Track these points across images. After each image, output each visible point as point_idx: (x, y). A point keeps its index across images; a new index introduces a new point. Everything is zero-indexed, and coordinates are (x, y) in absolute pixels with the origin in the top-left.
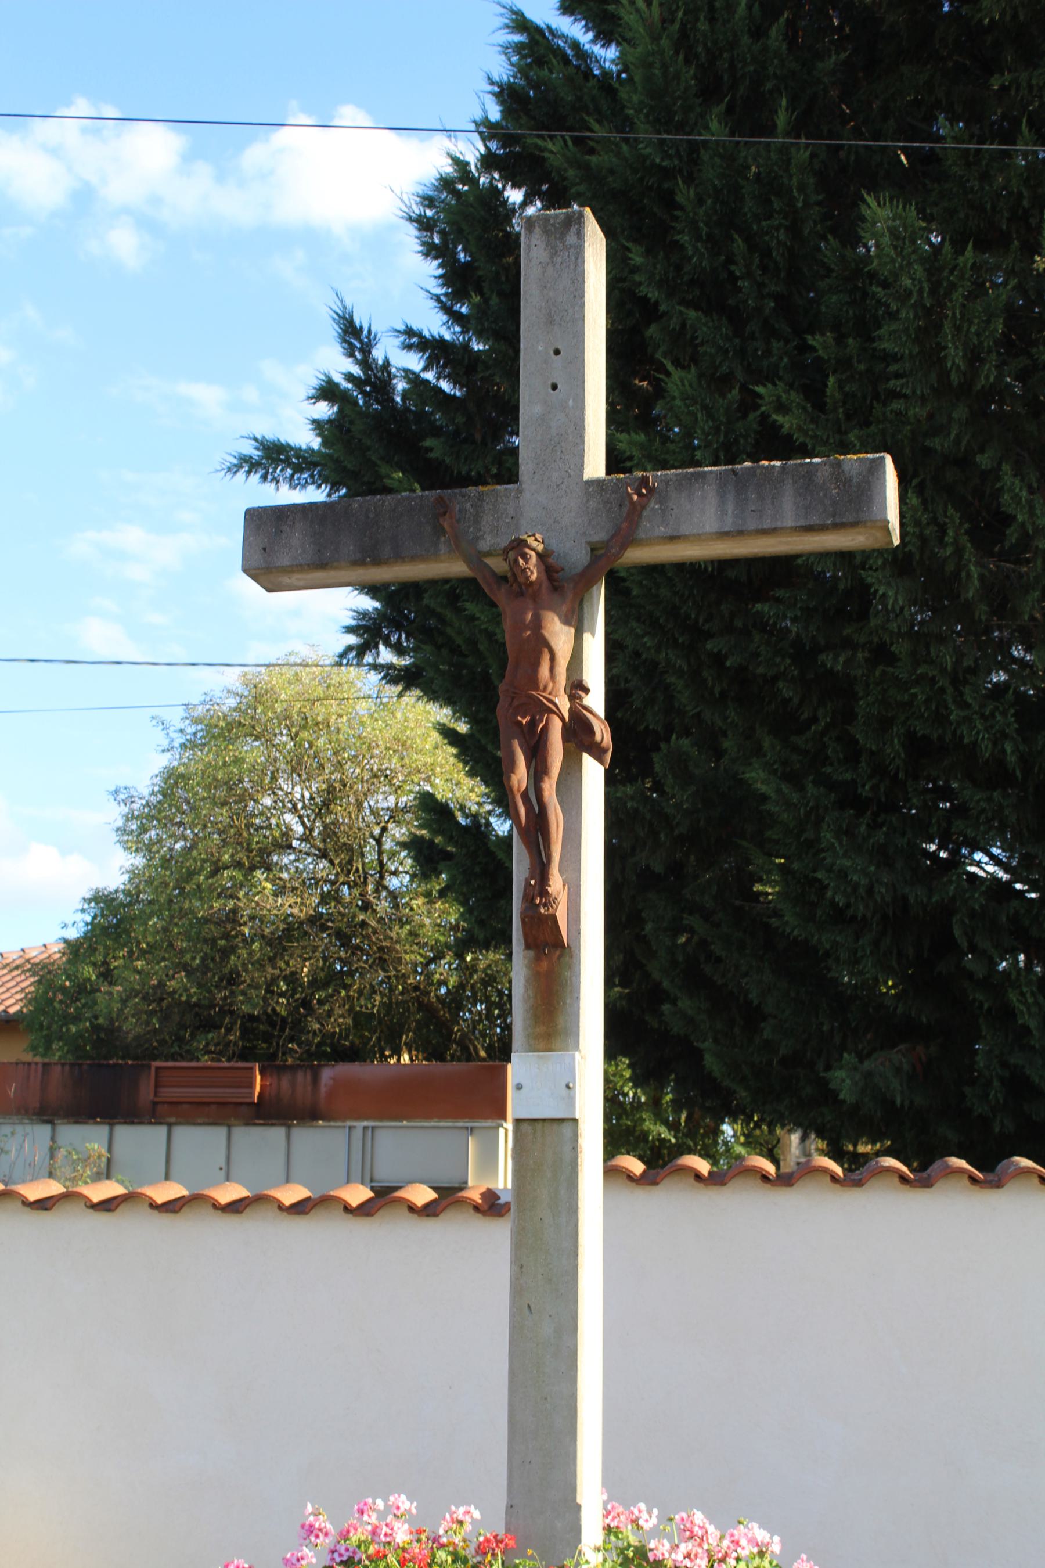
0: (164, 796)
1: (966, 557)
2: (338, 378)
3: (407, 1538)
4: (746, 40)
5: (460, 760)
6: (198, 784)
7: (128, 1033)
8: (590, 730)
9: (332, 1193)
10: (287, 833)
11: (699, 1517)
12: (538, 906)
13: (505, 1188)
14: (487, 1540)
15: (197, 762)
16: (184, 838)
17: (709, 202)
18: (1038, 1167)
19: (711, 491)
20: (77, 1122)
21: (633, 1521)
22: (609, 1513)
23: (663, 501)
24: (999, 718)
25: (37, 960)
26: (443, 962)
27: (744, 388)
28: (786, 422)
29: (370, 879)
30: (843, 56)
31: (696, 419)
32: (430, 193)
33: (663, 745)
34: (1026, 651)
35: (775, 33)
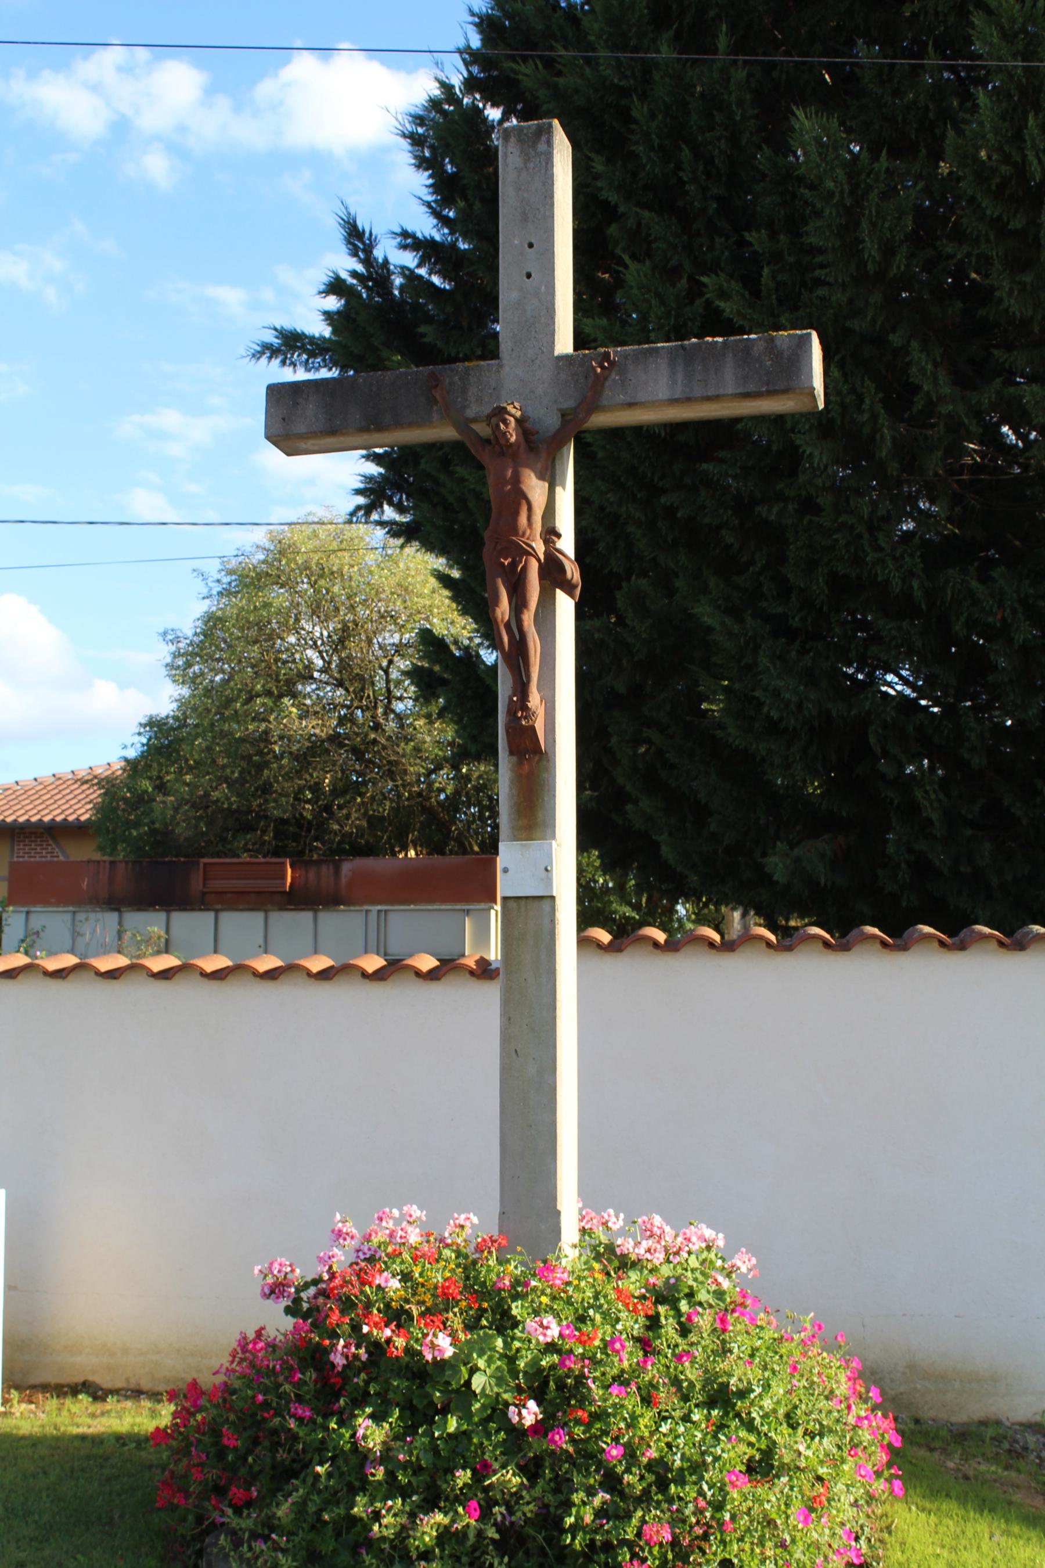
0: (205, 636)
1: (880, 421)
2: (344, 275)
3: (419, 1239)
6: (234, 626)
8: (562, 569)
9: (351, 962)
10: (309, 666)
11: (657, 1220)
12: (520, 718)
13: (496, 959)
14: (484, 1240)
16: (223, 671)
17: (660, 116)
18: (938, 933)
19: (662, 365)
20: (139, 910)
21: (603, 1224)
22: (583, 1218)
24: (907, 559)
25: (103, 776)
26: (442, 772)
27: (691, 278)
28: (728, 308)
29: (380, 704)
31: (651, 306)
32: (421, 113)
33: (624, 585)
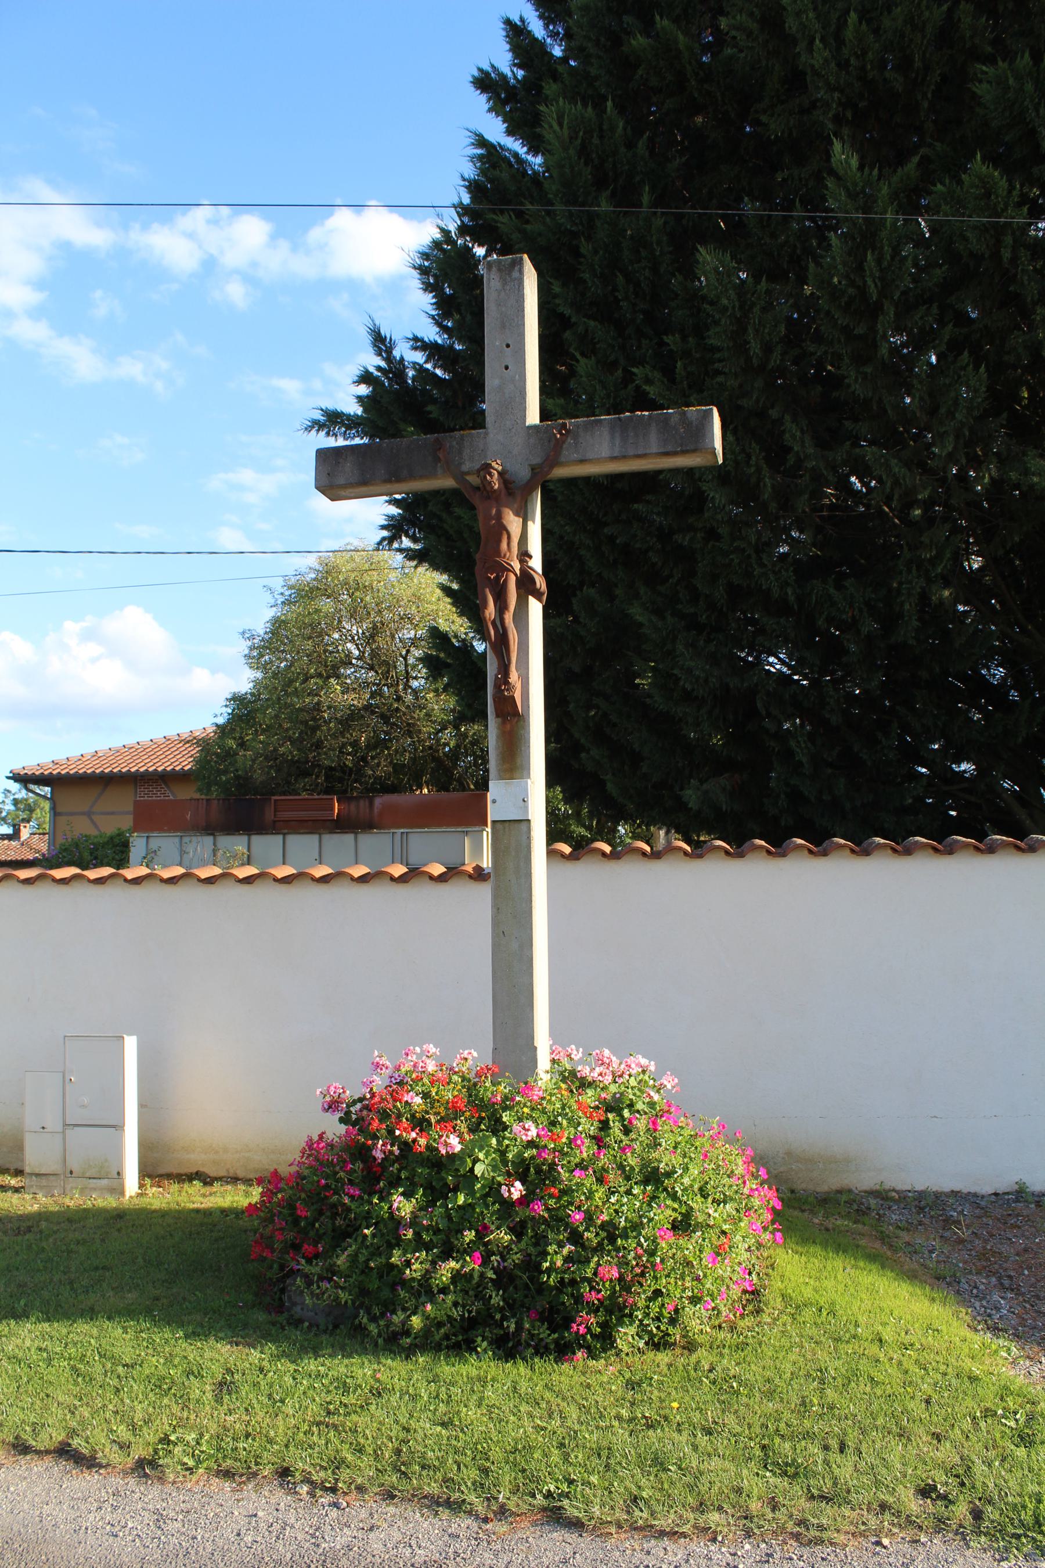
2: (372, 370)
3: (435, 1069)
4: (623, 150)
5: (454, 606)
6: (293, 626)
7: (256, 779)
10: (349, 655)
11: (607, 1052)
12: (503, 690)
13: (488, 867)
14: (482, 1069)
15: (292, 613)
17: (601, 252)
20: (228, 834)
21: (568, 1056)
23: (576, 438)
27: (625, 370)
28: (652, 391)
30: (684, 159)
34: (800, 533)
35: (641, 144)
